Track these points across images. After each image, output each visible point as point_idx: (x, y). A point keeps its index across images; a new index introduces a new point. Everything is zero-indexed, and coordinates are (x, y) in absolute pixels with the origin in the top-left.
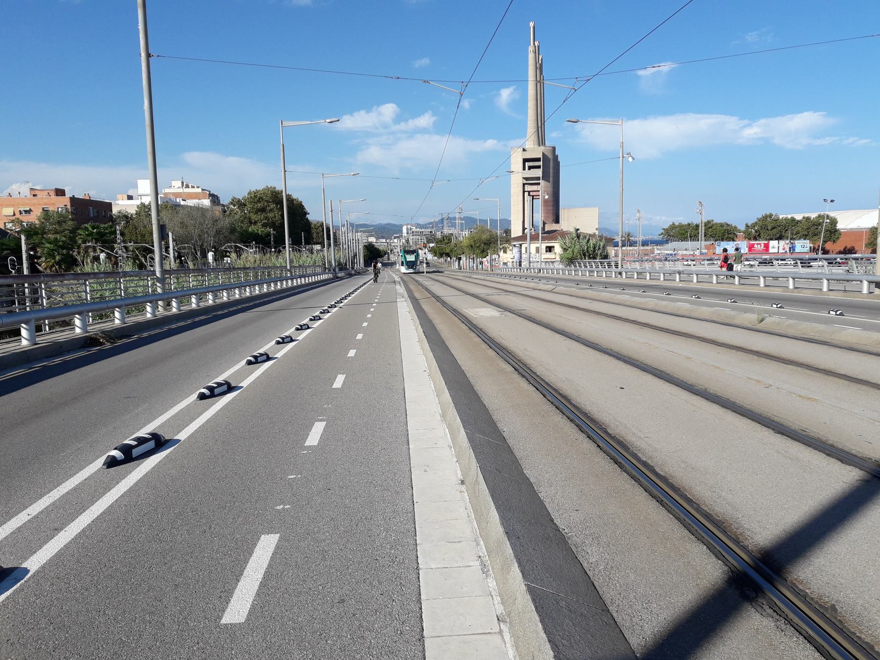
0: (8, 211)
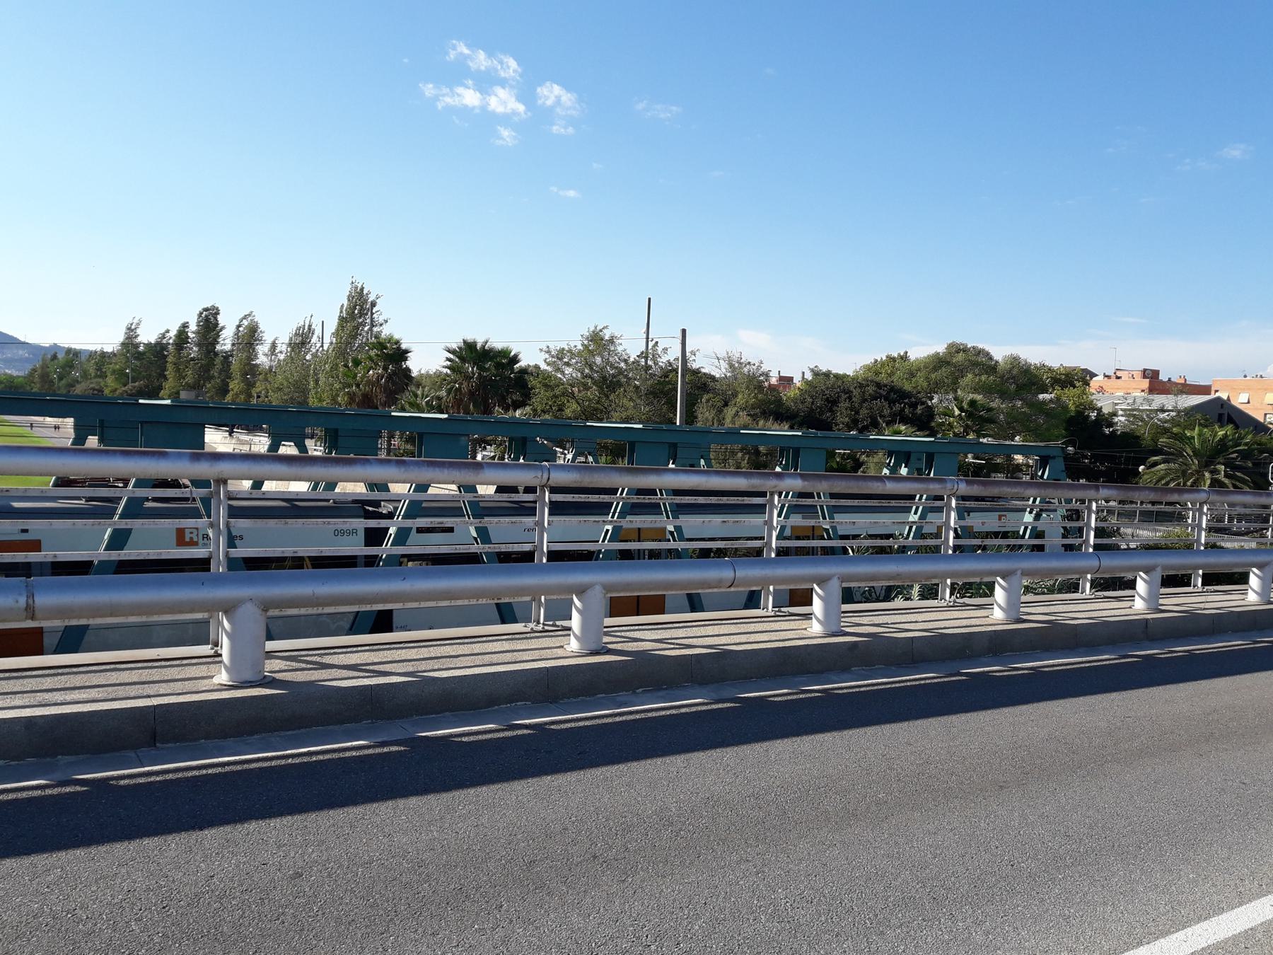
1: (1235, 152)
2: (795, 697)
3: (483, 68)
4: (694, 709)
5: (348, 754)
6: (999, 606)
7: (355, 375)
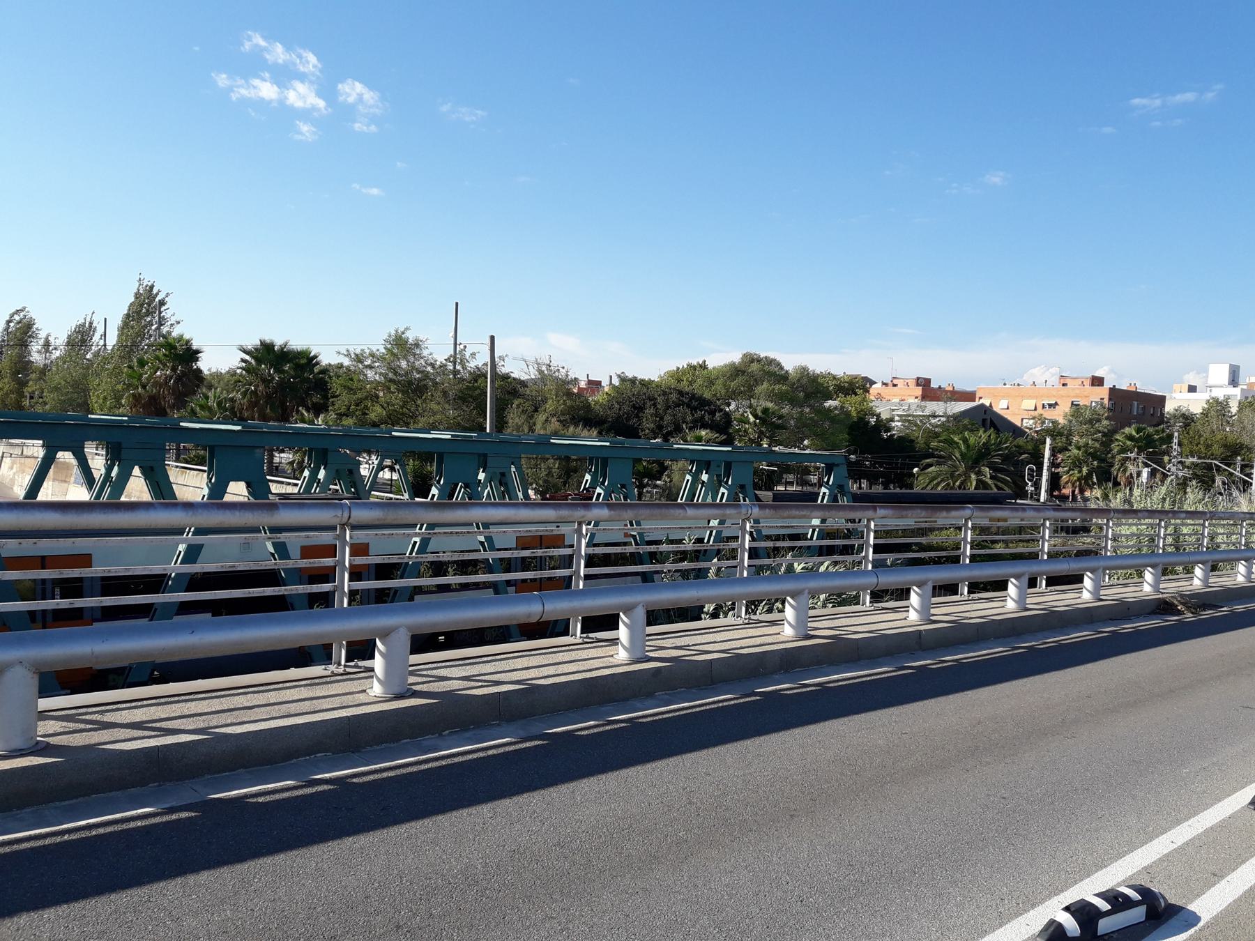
0: (1029, 404)
1: (996, 179)
2: (601, 729)
3: (280, 61)
4: (501, 750)
5: (132, 825)
6: (789, 623)
7: (141, 375)
